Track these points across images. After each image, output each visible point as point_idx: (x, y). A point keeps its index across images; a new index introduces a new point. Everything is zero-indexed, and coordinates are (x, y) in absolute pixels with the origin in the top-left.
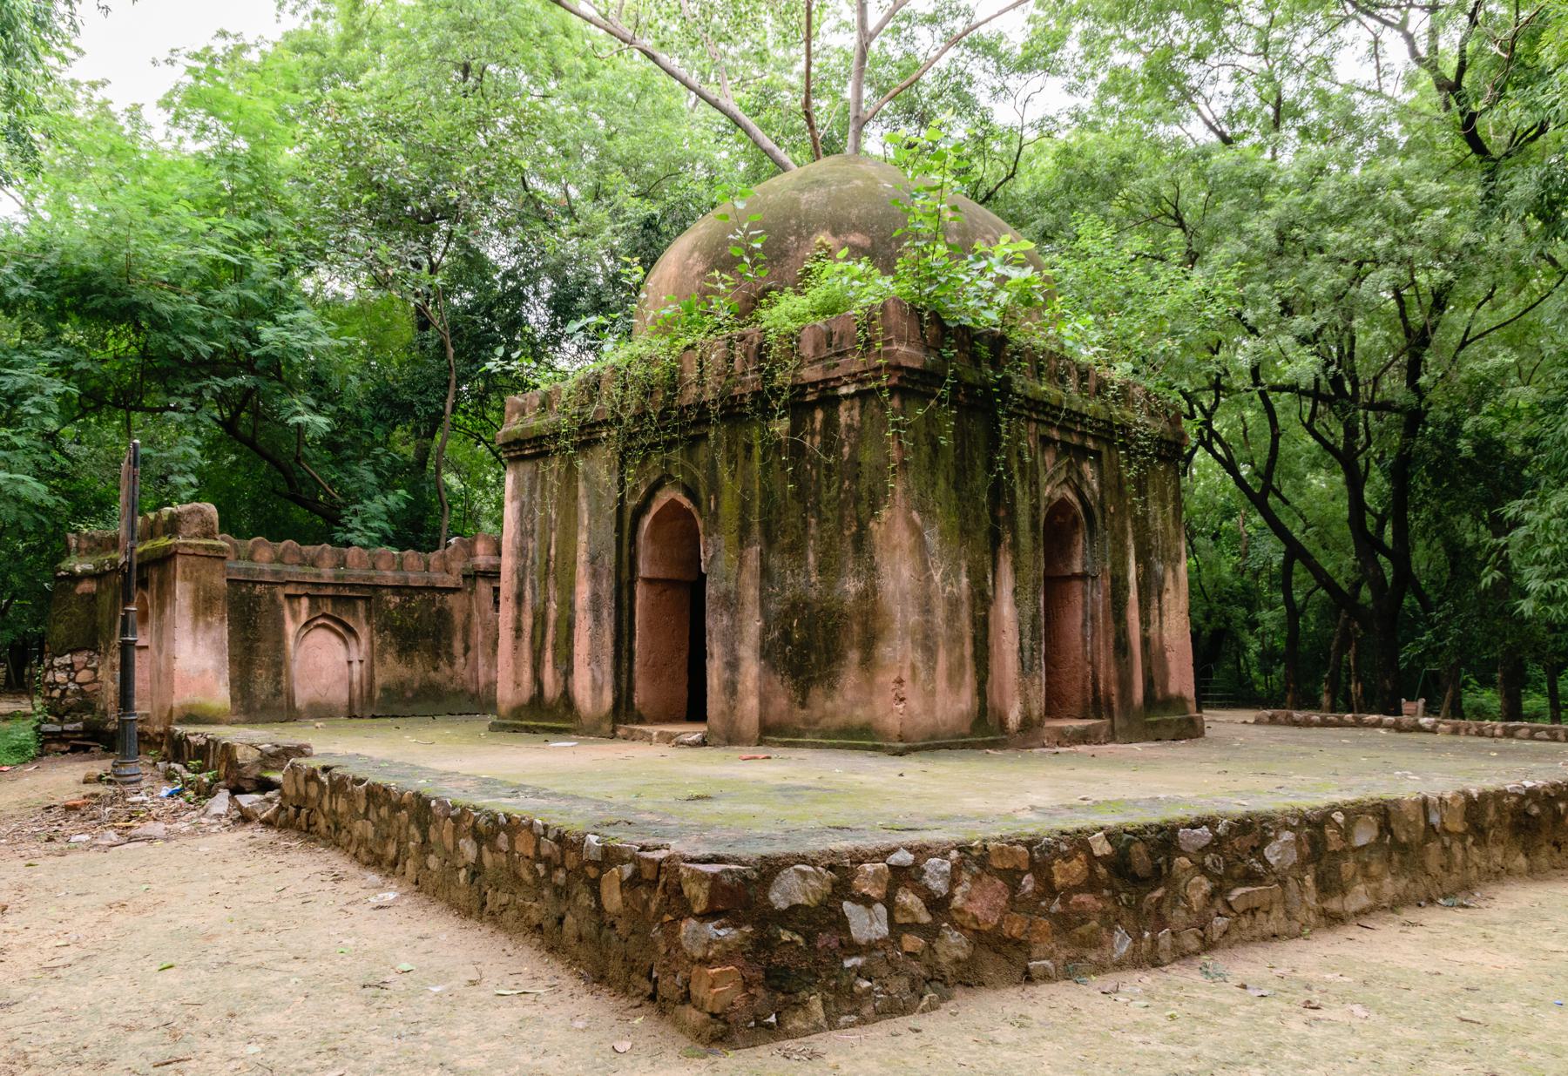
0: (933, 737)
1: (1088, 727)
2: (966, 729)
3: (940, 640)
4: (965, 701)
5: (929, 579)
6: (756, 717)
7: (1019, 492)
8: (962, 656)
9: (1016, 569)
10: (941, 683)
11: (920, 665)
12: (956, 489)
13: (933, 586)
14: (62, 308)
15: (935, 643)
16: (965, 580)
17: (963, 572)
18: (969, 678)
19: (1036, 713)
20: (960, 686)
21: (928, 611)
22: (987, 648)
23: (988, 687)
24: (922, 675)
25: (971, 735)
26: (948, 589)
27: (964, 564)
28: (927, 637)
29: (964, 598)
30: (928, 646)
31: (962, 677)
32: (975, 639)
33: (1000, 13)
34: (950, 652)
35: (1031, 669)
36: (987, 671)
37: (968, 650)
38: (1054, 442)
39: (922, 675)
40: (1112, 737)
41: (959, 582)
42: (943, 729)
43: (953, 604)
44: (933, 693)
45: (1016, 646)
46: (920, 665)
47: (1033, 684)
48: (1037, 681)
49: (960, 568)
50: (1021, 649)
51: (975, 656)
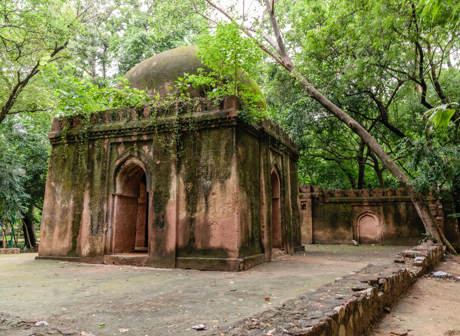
0: (50, 255)
1: (133, 258)
2: (65, 253)
3: (57, 223)
4: (66, 243)
5: (55, 203)
6: (325, 263)
7: (96, 167)
8: (67, 228)
9: (91, 196)
10: (55, 237)
11: (47, 231)
12: (73, 171)
13: (56, 205)
14: (396, 203)
15: (54, 224)
16: (72, 202)
17: (72, 199)
18: (69, 236)
19: (98, 250)
20: (63, 239)
21: (53, 214)
22: (79, 225)
23: (78, 239)
24: (48, 235)
25: (67, 256)
26: (63, 206)
27: (72, 196)
28: (51, 222)
29: (70, 208)
30: (51, 225)
31: (65, 235)
32: (73, 222)
33: (244, 8)
34: (61, 227)
35: (97, 233)
36: (78, 233)
37: (70, 226)
38: (121, 143)
39: (48, 235)
40: (148, 264)
41: (69, 203)
42: (55, 253)
43: (65, 211)
44: (52, 240)
45: (89, 224)
46: (47, 231)
47: (97, 239)
48: (100, 238)
49: (70, 198)
50: (92, 225)
51: (73, 228)
